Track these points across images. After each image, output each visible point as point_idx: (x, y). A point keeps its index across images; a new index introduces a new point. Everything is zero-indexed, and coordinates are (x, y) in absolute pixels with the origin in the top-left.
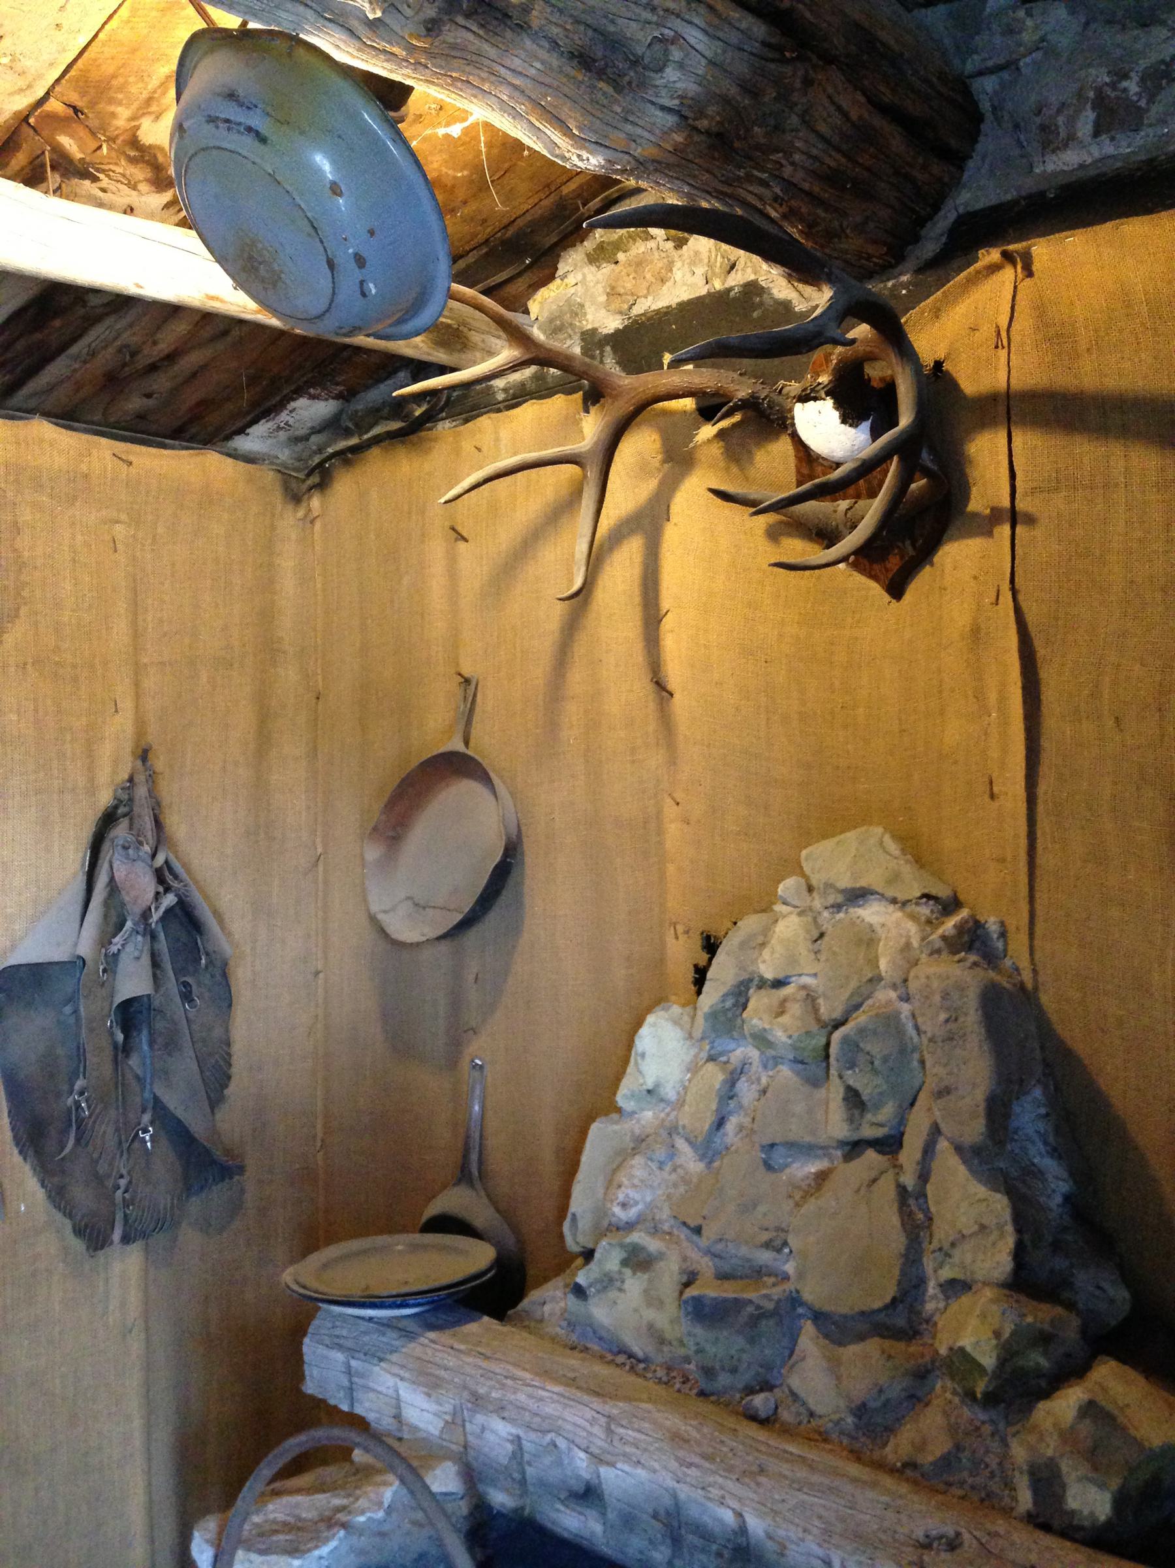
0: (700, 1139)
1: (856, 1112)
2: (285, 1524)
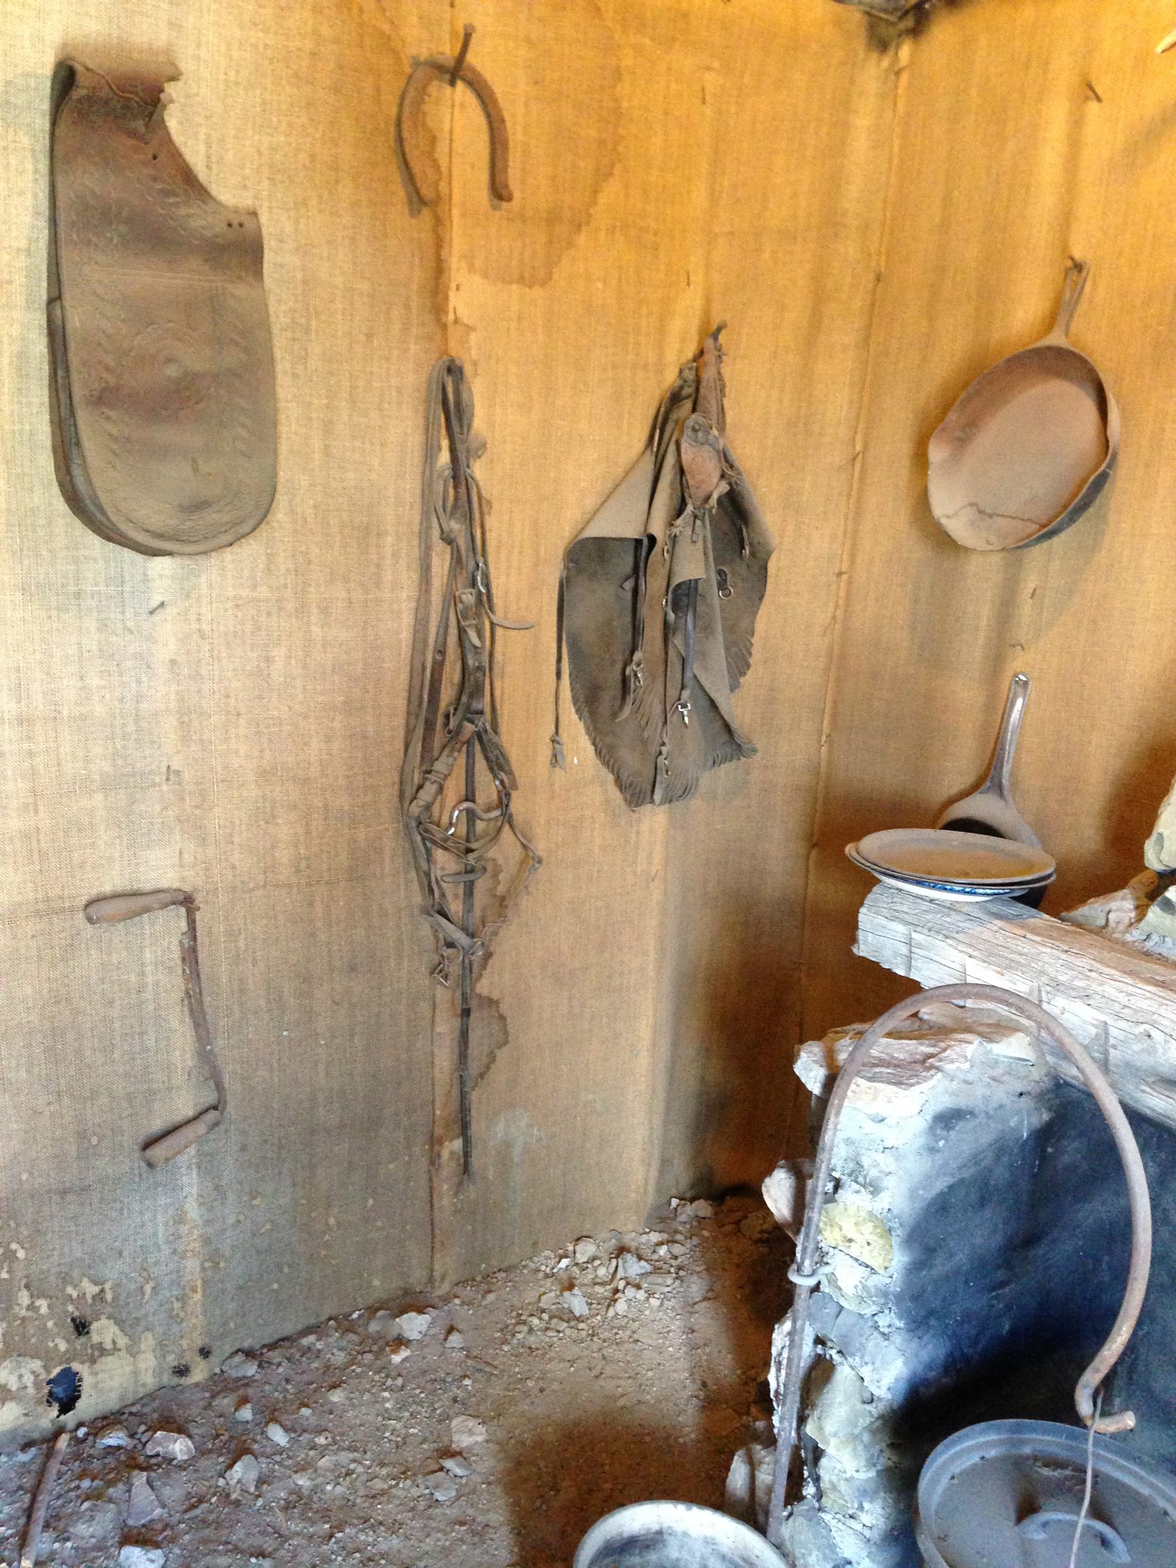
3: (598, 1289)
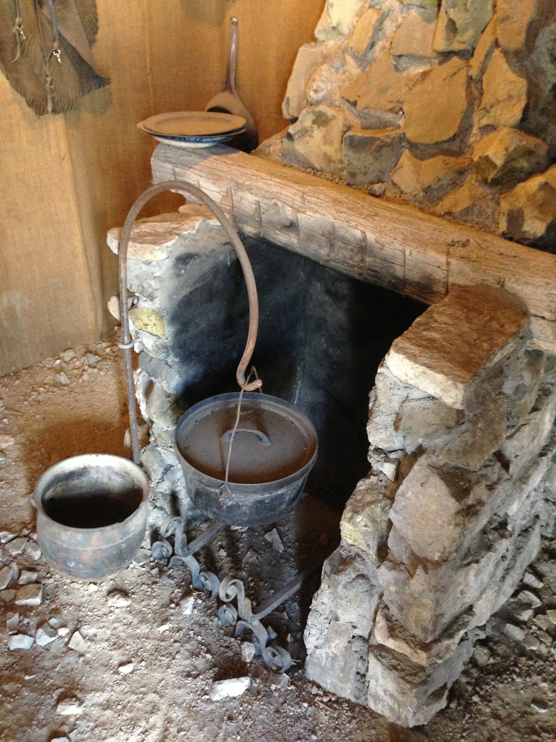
0: (360, 54)
1: (452, 34)
2: (150, 233)
3: (75, 371)
